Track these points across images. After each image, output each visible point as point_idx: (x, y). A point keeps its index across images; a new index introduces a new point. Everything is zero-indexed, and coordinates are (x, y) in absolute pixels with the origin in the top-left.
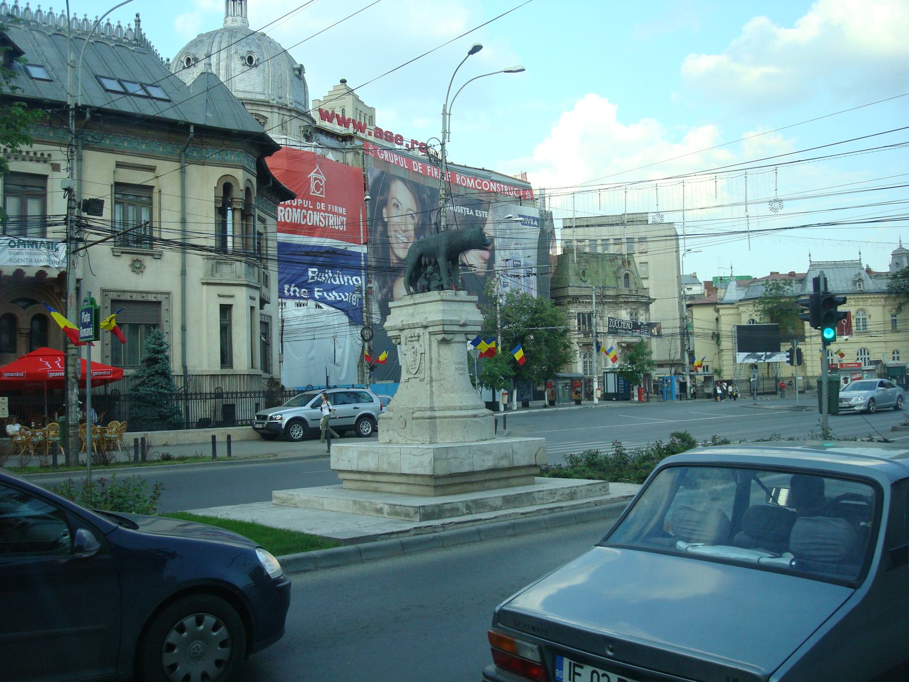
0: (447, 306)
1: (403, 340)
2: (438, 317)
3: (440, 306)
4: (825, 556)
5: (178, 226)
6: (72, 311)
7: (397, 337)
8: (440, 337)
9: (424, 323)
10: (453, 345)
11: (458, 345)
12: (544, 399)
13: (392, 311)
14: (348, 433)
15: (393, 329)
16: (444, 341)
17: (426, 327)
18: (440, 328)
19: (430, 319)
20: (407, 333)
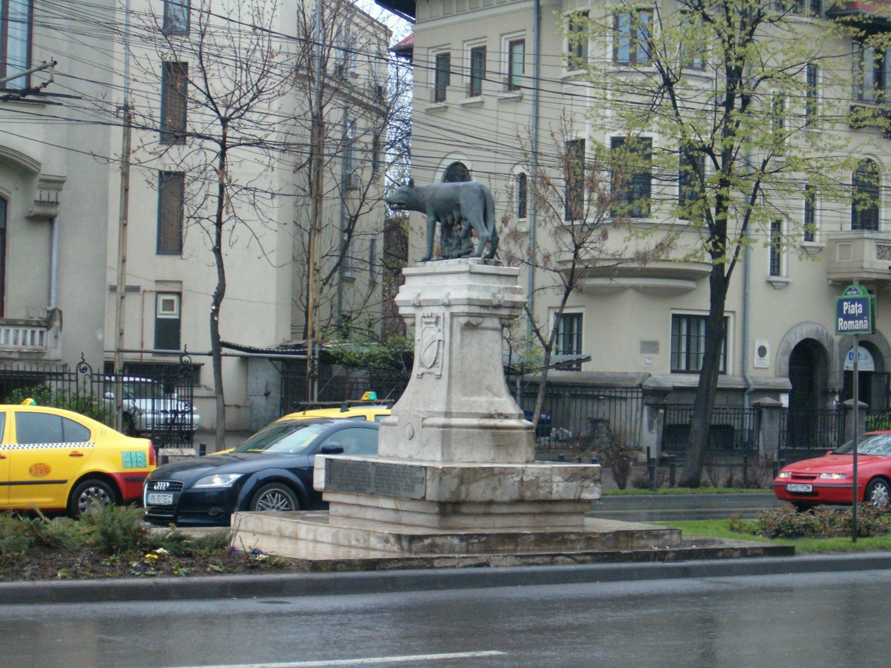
0: (478, 282)
1: (418, 320)
2: (463, 294)
3: (466, 280)
4: (533, 564)
5: (541, 99)
6: (572, 428)
7: (413, 316)
8: (463, 320)
9: (446, 301)
10: (480, 332)
11: (489, 333)
12: (172, 309)
13: (408, 281)
14: (144, 434)
15: (407, 304)
16: (469, 327)
17: (448, 305)
18: (465, 309)
19: (452, 296)
20: (427, 311)
